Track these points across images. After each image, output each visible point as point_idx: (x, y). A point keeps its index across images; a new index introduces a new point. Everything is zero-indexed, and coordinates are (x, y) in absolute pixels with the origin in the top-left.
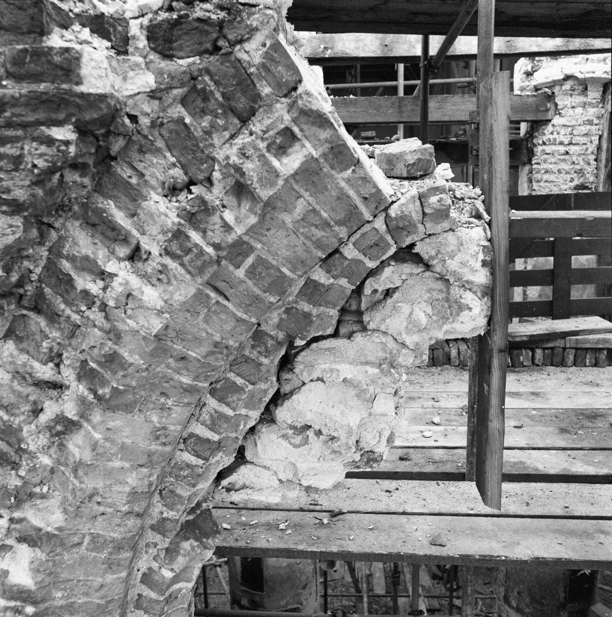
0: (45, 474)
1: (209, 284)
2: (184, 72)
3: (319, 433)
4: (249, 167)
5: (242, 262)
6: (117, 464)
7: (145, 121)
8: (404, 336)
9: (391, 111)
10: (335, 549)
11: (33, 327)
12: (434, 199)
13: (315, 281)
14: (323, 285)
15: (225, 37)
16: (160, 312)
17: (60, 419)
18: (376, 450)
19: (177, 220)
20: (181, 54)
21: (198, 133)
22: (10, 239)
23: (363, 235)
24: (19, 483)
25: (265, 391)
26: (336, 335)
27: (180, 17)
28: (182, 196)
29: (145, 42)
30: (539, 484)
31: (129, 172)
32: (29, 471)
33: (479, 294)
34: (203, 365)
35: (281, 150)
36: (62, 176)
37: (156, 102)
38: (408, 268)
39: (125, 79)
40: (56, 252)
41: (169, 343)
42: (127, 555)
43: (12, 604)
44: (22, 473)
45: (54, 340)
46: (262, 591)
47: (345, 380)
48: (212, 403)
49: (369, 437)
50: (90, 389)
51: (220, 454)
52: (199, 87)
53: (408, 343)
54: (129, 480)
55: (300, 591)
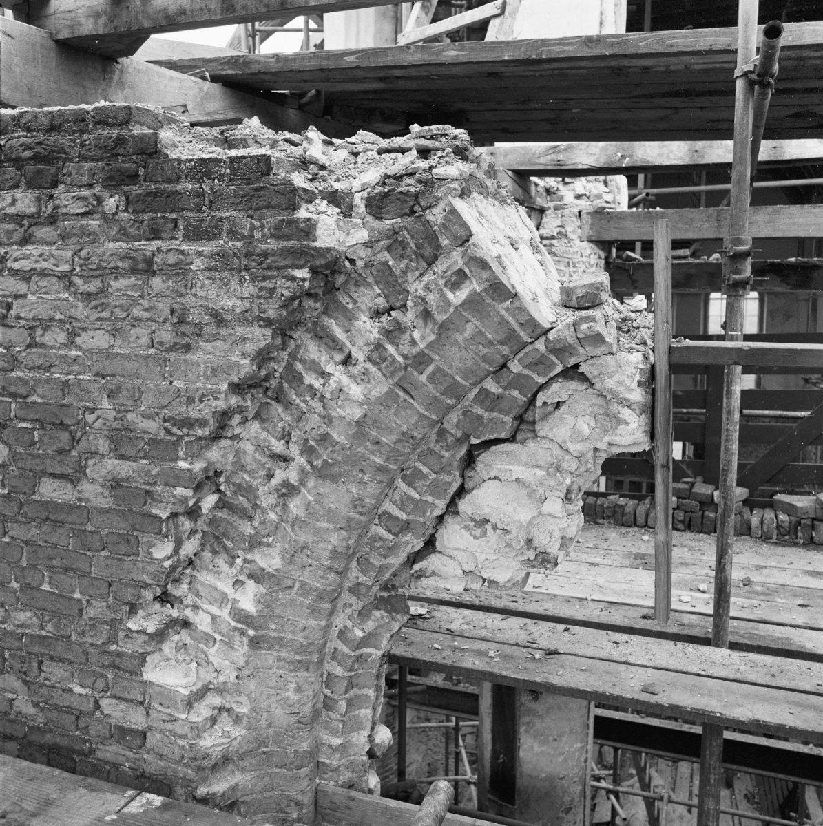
0: (272, 529)
1: (398, 384)
2: (389, 230)
3: (495, 527)
4: (432, 298)
5: (424, 369)
6: (324, 525)
7: (360, 263)
8: (569, 444)
9: (706, 225)
10: (539, 679)
11: (273, 412)
12: (584, 326)
13: (487, 390)
14: (493, 393)
15: (419, 204)
16: (361, 404)
17: (286, 483)
18: (549, 551)
19: (377, 336)
20: (387, 216)
21: (398, 273)
22: (262, 344)
23: (526, 354)
24: (253, 532)
25: (450, 484)
26: (512, 439)
27: (389, 191)
28: (384, 318)
29: (364, 209)
30: (798, 661)
31: (347, 300)
32: (261, 523)
33: (638, 411)
34: (393, 450)
35: (455, 286)
36: (300, 302)
37: (370, 250)
38: (573, 385)
39: (348, 234)
40: (293, 357)
41: (367, 429)
42: (328, 606)
43: (240, 626)
44: (255, 524)
45: (286, 422)
46: (513, 804)
47: (517, 480)
48: (400, 484)
49: (541, 536)
50: (308, 462)
51: (410, 535)
52: (400, 239)
53: (571, 451)
54: (332, 540)
55: (561, 815)
